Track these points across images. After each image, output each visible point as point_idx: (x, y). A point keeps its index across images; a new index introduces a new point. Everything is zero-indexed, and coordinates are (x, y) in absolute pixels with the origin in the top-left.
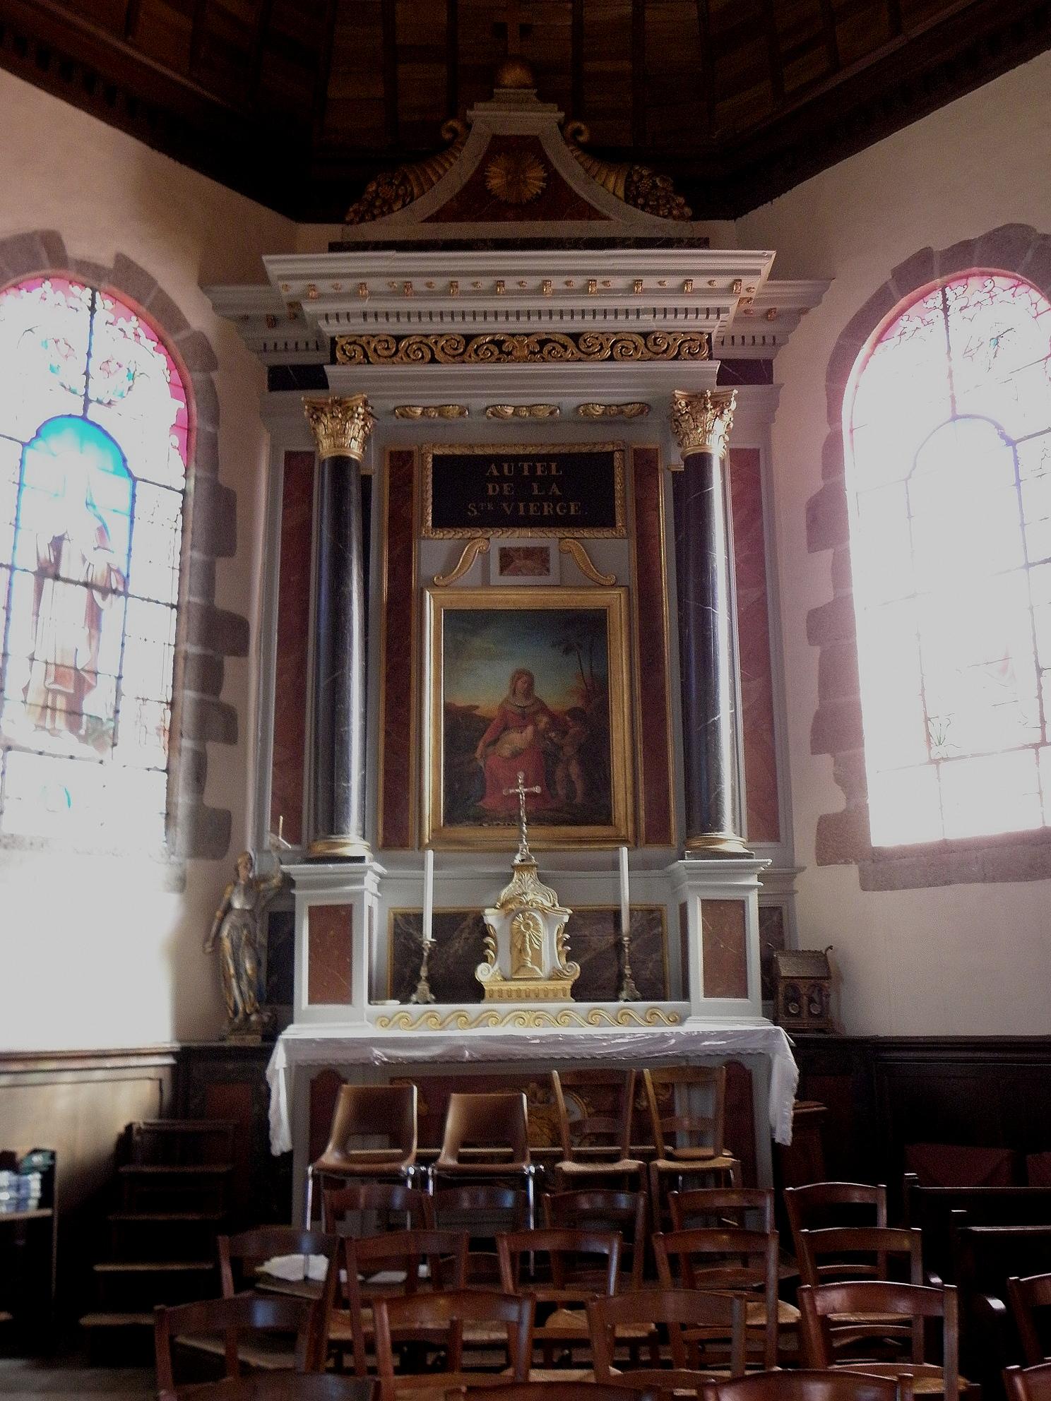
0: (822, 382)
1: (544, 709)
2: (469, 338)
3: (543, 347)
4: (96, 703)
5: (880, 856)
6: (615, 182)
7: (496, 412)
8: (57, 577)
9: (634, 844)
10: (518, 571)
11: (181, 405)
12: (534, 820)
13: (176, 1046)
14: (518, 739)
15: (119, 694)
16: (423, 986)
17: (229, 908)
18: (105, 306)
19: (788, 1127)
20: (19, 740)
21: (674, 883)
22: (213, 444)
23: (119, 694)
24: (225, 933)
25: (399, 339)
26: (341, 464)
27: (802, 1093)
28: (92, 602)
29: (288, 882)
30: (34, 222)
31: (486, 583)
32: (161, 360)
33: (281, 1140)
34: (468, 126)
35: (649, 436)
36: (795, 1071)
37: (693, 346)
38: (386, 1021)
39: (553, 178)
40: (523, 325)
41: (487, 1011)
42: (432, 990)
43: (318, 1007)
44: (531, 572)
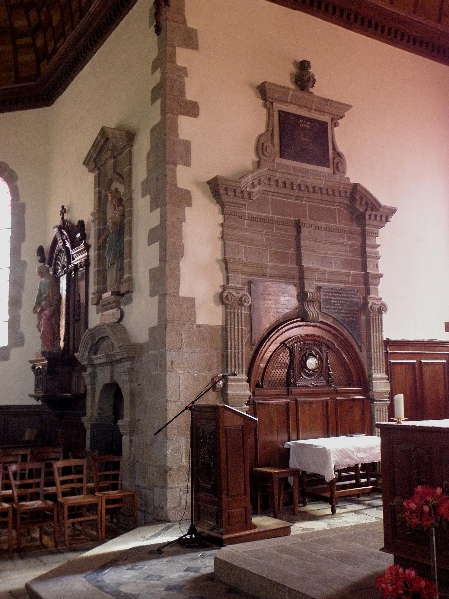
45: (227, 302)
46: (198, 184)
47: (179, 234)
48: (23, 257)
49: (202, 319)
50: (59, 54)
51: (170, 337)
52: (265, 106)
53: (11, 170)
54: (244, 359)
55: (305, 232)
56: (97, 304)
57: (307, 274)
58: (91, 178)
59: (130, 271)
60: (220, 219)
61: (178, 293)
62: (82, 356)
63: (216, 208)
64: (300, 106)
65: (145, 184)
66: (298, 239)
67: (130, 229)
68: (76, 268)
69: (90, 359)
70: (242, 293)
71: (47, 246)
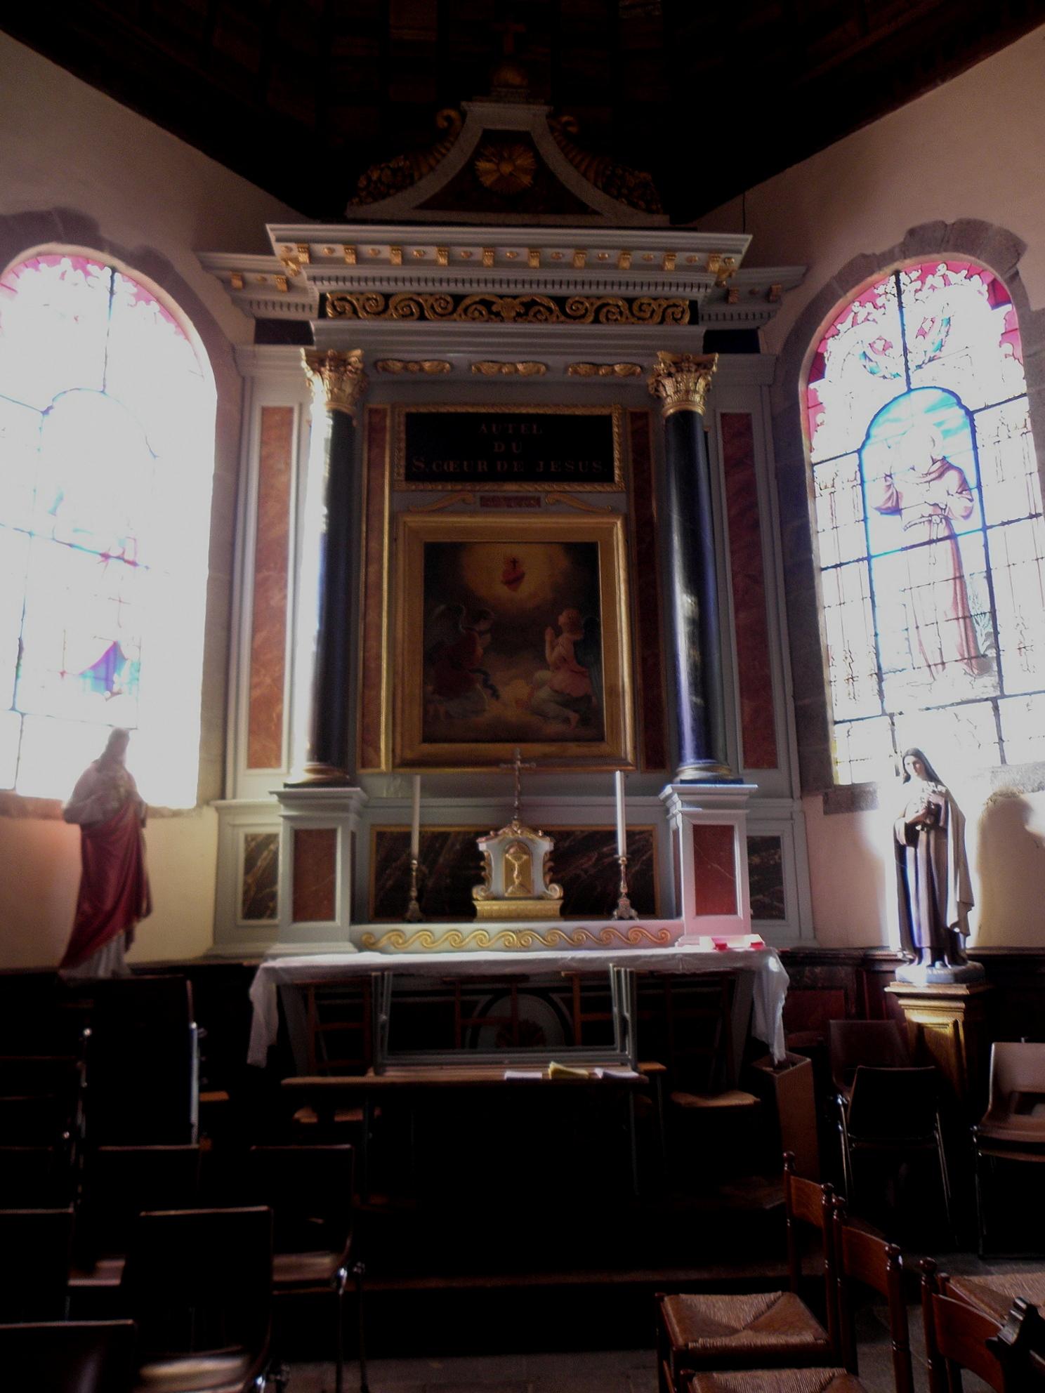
34: (463, 115)
41: (478, 930)
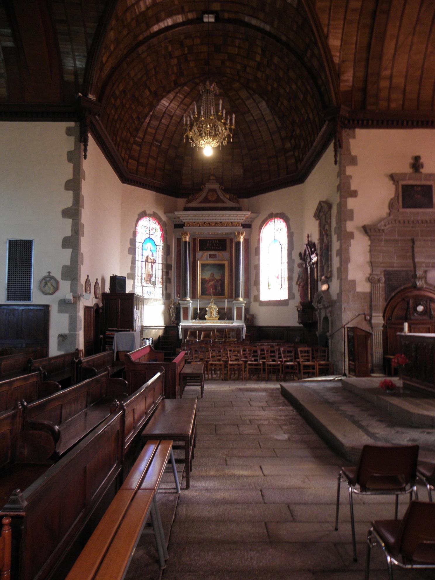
0: (258, 229)
1: (215, 279)
2: (205, 222)
3: (216, 224)
4: (153, 279)
5: (262, 302)
6: (228, 196)
7: (209, 233)
8: (147, 262)
9: (228, 298)
10: (211, 258)
11: (162, 232)
12: (214, 295)
13: (165, 326)
14: (212, 283)
15: (156, 278)
16: (198, 318)
17: (171, 307)
18: (151, 219)
19: (245, 337)
20: (145, 285)
21: (233, 304)
22: (167, 238)
23: (156, 278)
24: (171, 310)
25: (194, 222)
26: (186, 242)
27: (247, 332)
28: (152, 264)
29: (179, 303)
30: (142, 210)
31: (207, 260)
32: (159, 226)
33: (181, 337)
35: (232, 236)
36: (246, 330)
37: (237, 225)
38: (193, 323)
39: (218, 196)
40: (213, 221)
42: (199, 318)
43: (184, 321)
44: (213, 258)
45: (372, 281)
46: (357, 228)
47: (348, 252)
48: (293, 258)
49: (359, 289)
50: (305, 160)
51: (344, 298)
52: (394, 184)
53: (287, 216)
54: (381, 307)
55: (417, 244)
56: (320, 281)
57: (417, 265)
58: (317, 222)
59: (331, 268)
60: (369, 243)
61: (347, 278)
62: (314, 304)
63: (367, 238)
64: (55, 448)
65: (335, 228)
66: (413, 248)
67: (331, 249)
68: (313, 264)
69: (318, 307)
70: (379, 277)
71: (303, 252)
